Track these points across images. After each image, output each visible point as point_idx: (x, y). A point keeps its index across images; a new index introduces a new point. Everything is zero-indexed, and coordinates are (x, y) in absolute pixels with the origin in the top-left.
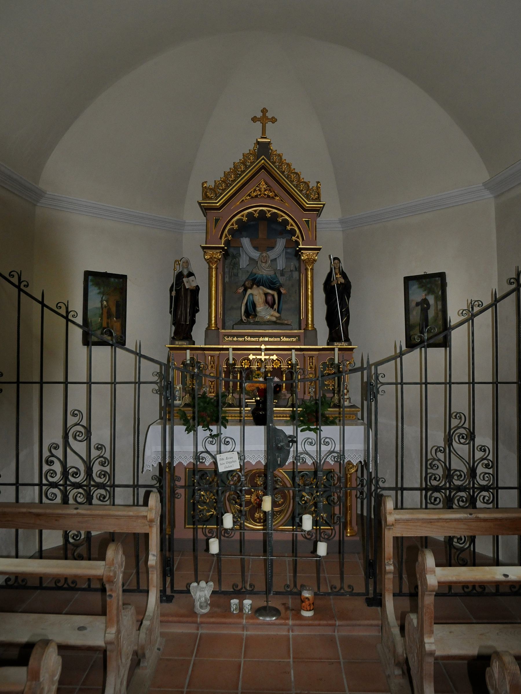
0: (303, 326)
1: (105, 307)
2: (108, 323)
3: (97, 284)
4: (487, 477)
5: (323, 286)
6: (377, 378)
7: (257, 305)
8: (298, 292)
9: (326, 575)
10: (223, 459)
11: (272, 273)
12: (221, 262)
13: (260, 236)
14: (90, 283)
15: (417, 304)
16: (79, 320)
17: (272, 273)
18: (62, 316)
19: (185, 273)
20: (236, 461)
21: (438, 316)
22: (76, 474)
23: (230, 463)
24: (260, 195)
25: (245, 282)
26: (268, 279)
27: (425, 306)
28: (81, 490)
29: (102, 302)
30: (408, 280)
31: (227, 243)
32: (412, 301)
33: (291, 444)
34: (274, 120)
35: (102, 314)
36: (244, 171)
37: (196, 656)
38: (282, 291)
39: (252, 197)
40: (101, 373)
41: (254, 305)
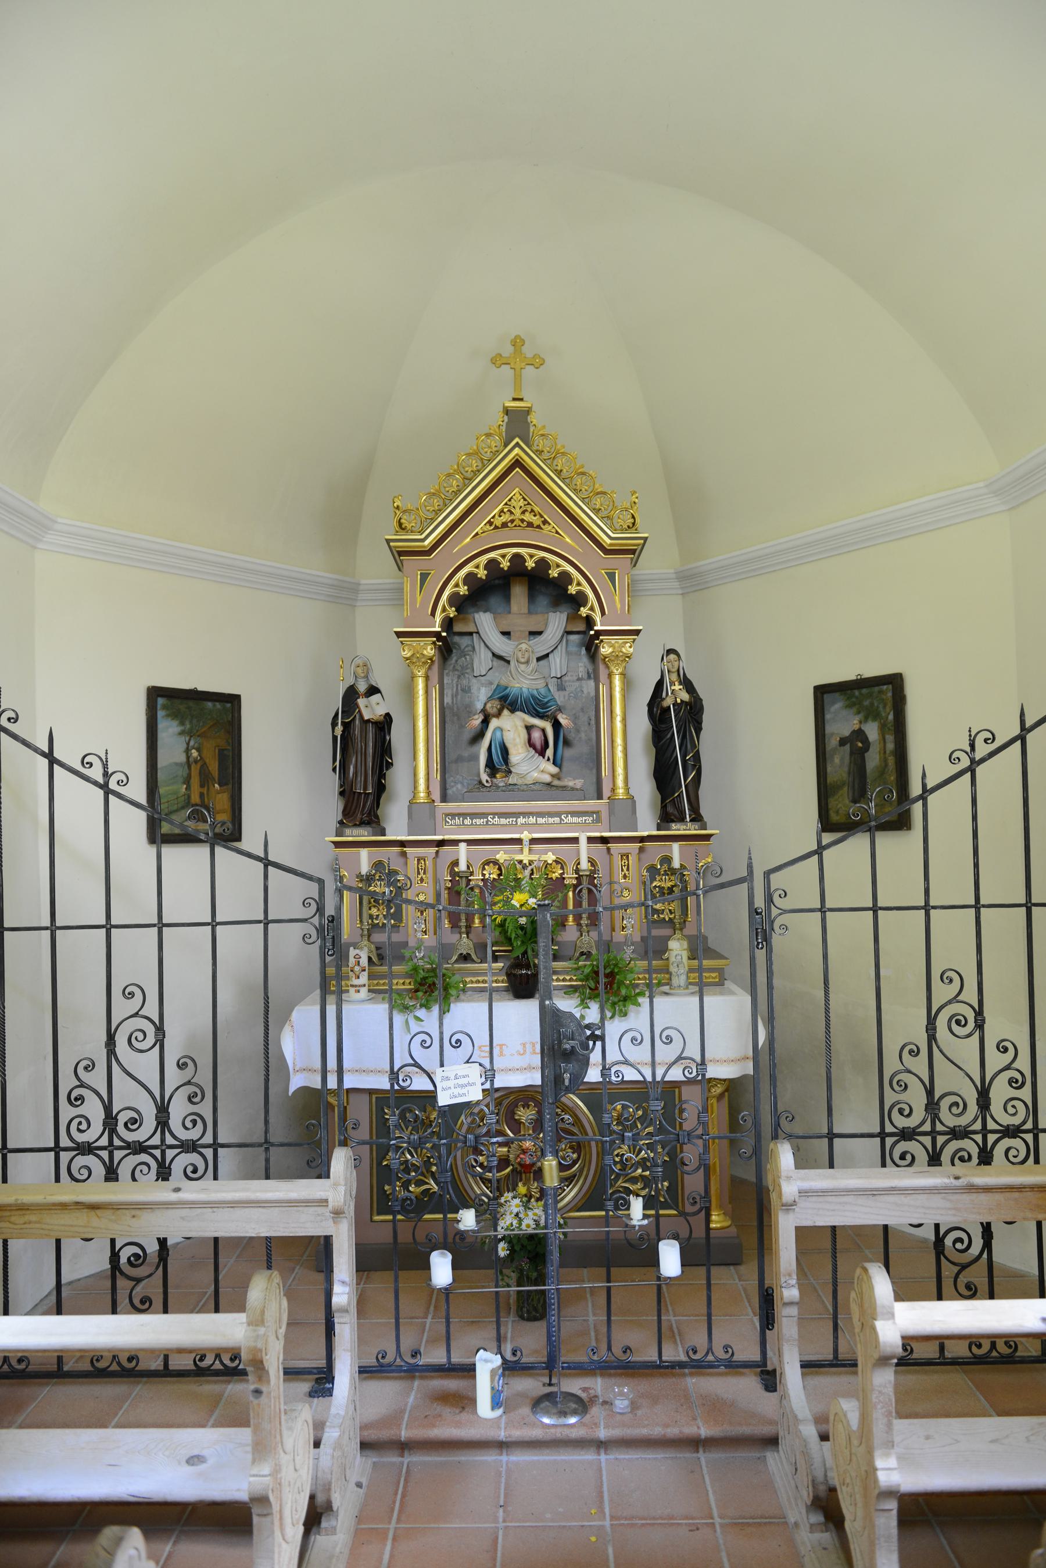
0: (606, 792)
1: (196, 762)
2: (202, 795)
3: (175, 715)
4: (1013, 1106)
5: (647, 708)
6: (769, 900)
7: (512, 751)
8: (593, 722)
9: (672, 1318)
10: (448, 1079)
11: (540, 684)
12: (436, 667)
13: (514, 607)
14: (160, 714)
15: (843, 742)
16: (138, 790)
17: (540, 684)
18: (95, 783)
19: (362, 687)
20: (474, 1084)
21: (886, 765)
22: (134, 1123)
23: (462, 1086)
24: (512, 521)
25: (485, 704)
26: (533, 696)
27: (860, 745)
28: (144, 1157)
29: (187, 751)
30: (822, 692)
31: (448, 624)
32: (832, 734)
33: (591, 1043)
34: (538, 362)
35: (189, 776)
36: (479, 471)
37: (398, 1521)
38: (562, 721)
39: (496, 527)
40: (186, 900)
41: (505, 751)
